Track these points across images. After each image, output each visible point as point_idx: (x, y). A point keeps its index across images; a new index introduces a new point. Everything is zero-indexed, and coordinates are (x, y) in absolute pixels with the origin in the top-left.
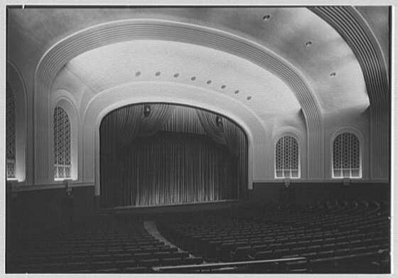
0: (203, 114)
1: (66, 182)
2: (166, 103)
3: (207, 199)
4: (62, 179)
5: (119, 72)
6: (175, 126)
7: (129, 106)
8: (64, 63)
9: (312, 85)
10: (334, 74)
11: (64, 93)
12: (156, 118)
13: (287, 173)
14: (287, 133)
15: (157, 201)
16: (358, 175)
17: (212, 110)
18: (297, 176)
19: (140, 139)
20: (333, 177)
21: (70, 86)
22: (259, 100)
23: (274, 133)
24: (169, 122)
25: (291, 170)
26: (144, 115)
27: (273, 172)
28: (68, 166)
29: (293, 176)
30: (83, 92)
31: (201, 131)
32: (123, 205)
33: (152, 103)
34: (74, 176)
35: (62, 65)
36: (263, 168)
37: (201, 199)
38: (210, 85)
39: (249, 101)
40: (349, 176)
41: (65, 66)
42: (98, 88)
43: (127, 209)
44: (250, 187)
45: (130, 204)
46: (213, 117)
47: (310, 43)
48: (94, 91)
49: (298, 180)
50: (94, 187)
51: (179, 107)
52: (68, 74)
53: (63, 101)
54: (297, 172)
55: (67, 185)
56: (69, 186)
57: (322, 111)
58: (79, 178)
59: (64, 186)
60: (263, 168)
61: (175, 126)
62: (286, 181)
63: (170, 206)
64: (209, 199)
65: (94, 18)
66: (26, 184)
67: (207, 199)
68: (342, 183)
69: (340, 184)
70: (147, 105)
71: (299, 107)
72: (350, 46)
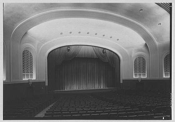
0: (96, 49)
1: (29, 80)
2: (77, 45)
3: (99, 87)
4: (28, 79)
5: (51, 35)
6: (82, 55)
7: (61, 47)
8: (26, 32)
9: (148, 30)
10: (160, 24)
11: (30, 45)
12: (73, 52)
13: (140, 75)
14: (141, 55)
15: (75, 88)
16: (145, 77)
17: (107, 48)
18: (145, 77)
19: (64, 62)
20: (164, 77)
21: (30, 41)
22: (123, 41)
23: (133, 56)
24: (79, 54)
25: (142, 73)
26: (67, 51)
27: (133, 74)
28: (32, 74)
29: (143, 76)
30: (158, 48)
31: (95, 56)
32: (59, 89)
33: (71, 46)
34: (34, 78)
35: (25, 33)
36: (127, 72)
37: (97, 87)
38: (89, 34)
39: (118, 41)
40: (141, 76)
41: (26, 33)
42: (45, 41)
43: (61, 91)
44: (121, 82)
45: (63, 89)
46: (101, 50)
47: (142, 10)
48: (43, 43)
49: (145, 78)
50: (45, 82)
51: (84, 46)
52: (29, 36)
53: (28, 48)
54: (145, 74)
55: (29, 81)
56: (30, 82)
57: (157, 43)
58: (36, 78)
59: (28, 82)
60: (127, 72)
61: (82, 55)
62: (139, 79)
63: (92, 90)
64: (100, 87)
65: (32, 13)
66: (6, 81)
67: (99, 87)
68: (138, 80)
69: (136, 81)
70: (68, 46)
71: (144, 42)
72: (164, 9)
